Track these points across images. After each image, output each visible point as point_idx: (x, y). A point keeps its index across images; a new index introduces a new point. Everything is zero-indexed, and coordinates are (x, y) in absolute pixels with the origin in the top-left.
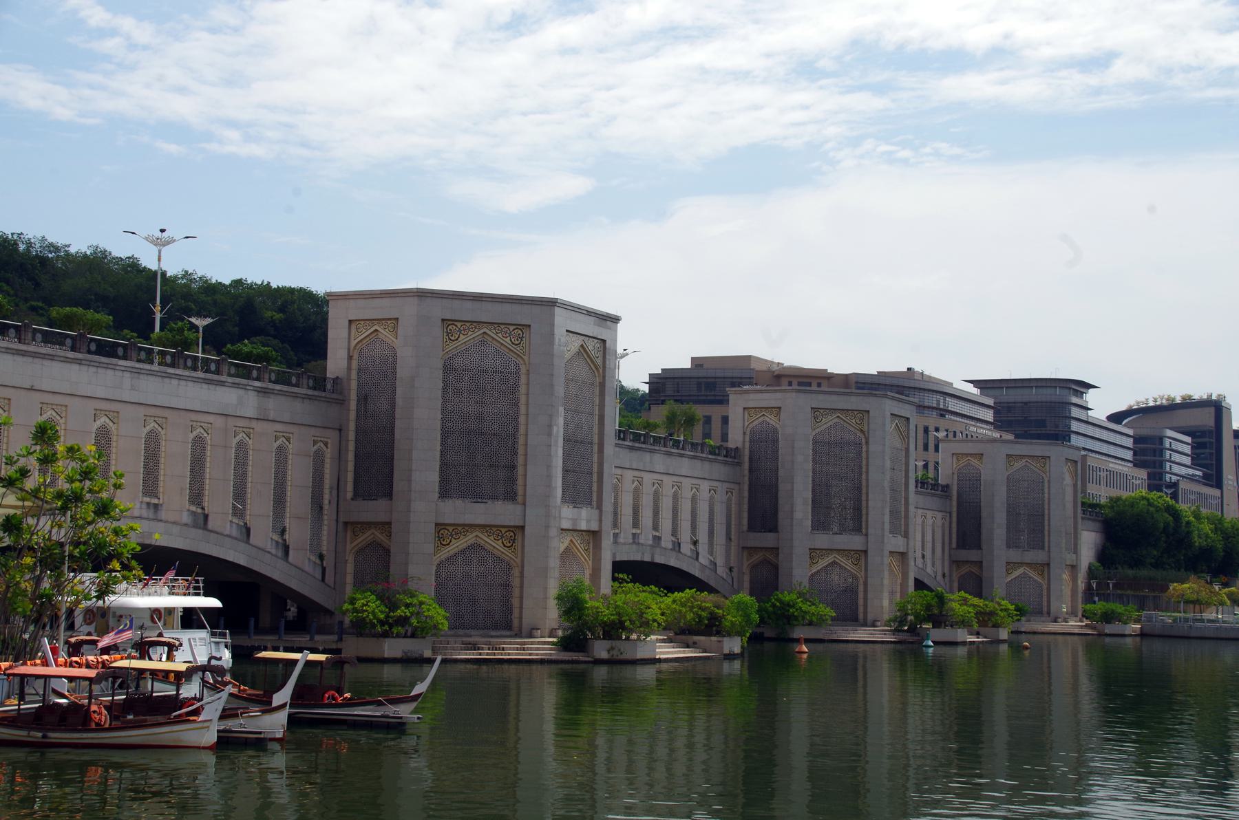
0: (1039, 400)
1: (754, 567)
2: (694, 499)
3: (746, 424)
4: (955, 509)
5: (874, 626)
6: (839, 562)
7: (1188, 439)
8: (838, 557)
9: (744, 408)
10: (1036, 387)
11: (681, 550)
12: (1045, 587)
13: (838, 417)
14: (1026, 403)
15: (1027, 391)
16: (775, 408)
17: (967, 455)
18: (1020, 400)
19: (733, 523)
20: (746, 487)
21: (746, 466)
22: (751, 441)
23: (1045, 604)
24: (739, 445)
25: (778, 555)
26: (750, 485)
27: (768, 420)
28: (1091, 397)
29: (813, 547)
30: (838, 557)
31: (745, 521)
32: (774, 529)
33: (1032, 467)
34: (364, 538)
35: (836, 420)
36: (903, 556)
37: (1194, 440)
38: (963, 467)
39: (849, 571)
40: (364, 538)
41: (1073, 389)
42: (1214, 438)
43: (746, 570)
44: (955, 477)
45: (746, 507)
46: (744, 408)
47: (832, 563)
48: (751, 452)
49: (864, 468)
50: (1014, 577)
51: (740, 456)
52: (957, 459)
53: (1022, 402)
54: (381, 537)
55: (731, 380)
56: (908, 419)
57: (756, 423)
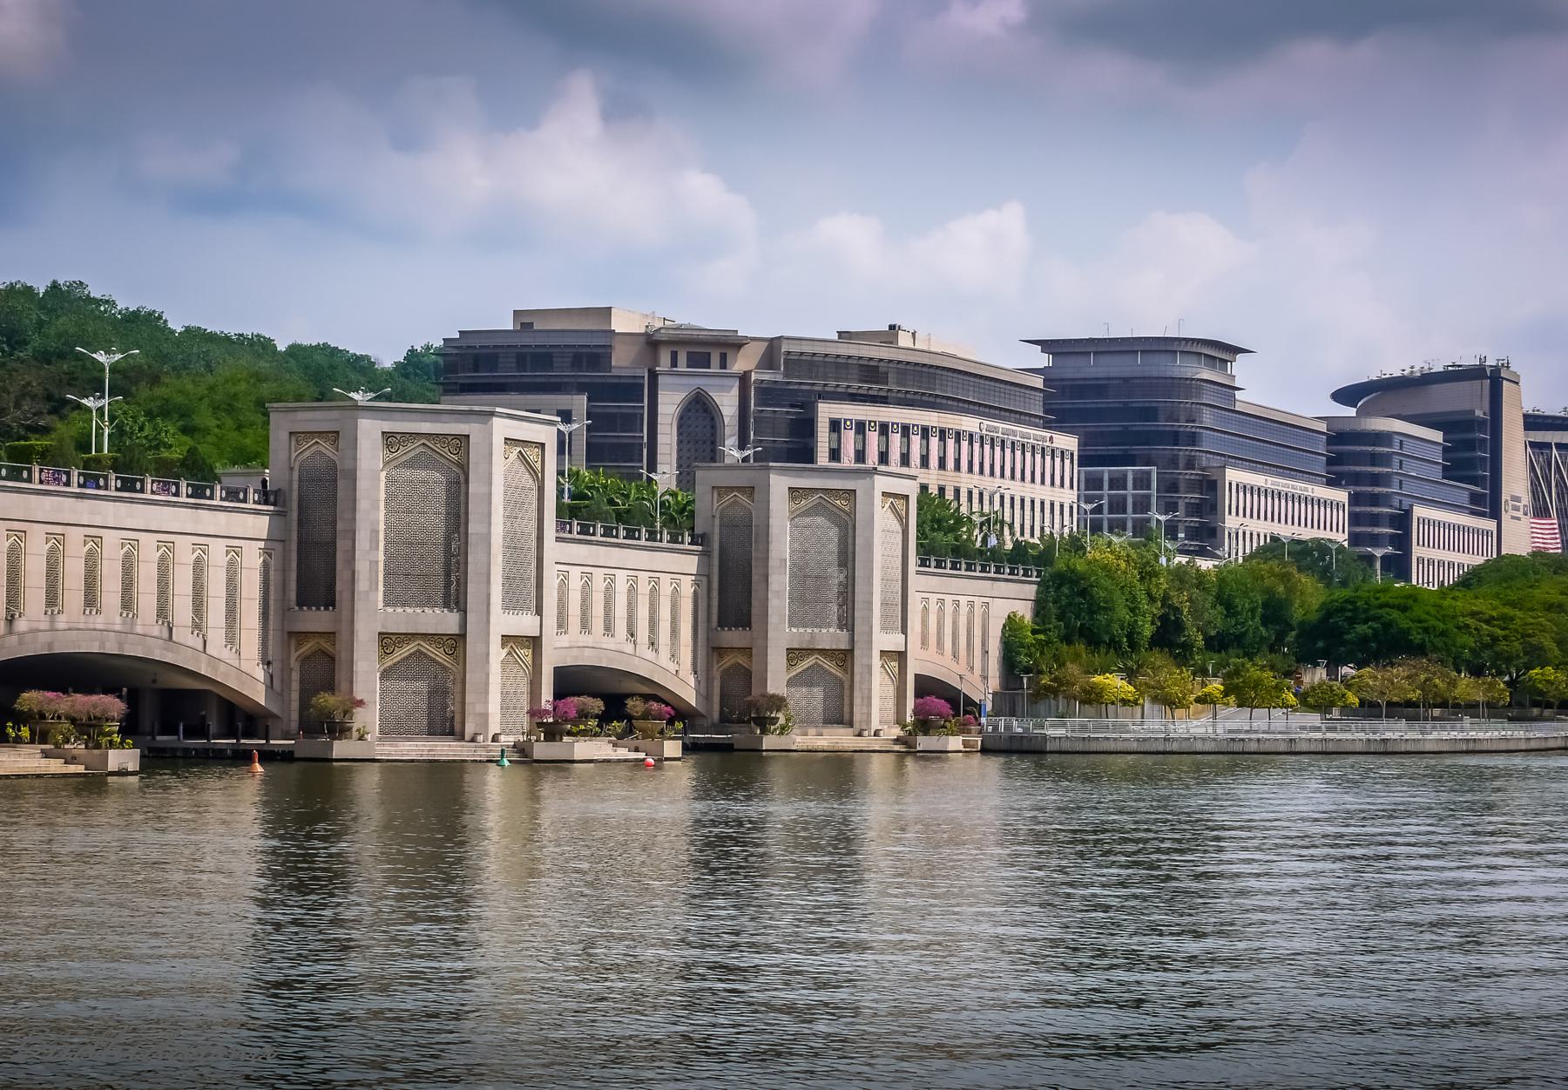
0: (1147, 374)
1: (305, 660)
2: (199, 567)
3: (294, 455)
4: (716, 570)
5: (473, 740)
6: (425, 651)
7: (1437, 436)
8: (424, 645)
9: (291, 433)
10: (1096, 353)
11: (174, 638)
12: (847, 685)
13: (424, 444)
14: (1126, 380)
15: (1127, 359)
16: (330, 432)
17: (732, 489)
18: (1117, 375)
19: (272, 597)
20: (294, 546)
21: (295, 515)
22: (300, 481)
23: (846, 709)
24: (283, 485)
25: (751, 656)
26: (300, 542)
27: (324, 451)
28: (1240, 369)
29: (385, 631)
30: (424, 645)
31: (293, 595)
32: (330, 602)
33: (828, 505)
34: (308, 647)
35: (422, 449)
36: (901, 656)
37: (1450, 437)
38: (728, 506)
39: (440, 664)
40: (308, 647)
41: (1206, 355)
42: (1488, 433)
43: (295, 664)
44: (717, 522)
45: (293, 576)
46: (291, 433)
47: (414, 653)
48: (300, 496)
49: (462, 516)
50: (801, 669)
51: (284, 501)
52: (719, 494)
53: (1120, 378)
54: (327, 646)
55: (574, 350)
56: (543, 445)
57: (307, 454)
